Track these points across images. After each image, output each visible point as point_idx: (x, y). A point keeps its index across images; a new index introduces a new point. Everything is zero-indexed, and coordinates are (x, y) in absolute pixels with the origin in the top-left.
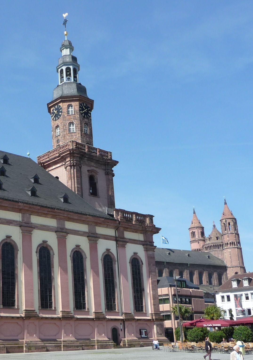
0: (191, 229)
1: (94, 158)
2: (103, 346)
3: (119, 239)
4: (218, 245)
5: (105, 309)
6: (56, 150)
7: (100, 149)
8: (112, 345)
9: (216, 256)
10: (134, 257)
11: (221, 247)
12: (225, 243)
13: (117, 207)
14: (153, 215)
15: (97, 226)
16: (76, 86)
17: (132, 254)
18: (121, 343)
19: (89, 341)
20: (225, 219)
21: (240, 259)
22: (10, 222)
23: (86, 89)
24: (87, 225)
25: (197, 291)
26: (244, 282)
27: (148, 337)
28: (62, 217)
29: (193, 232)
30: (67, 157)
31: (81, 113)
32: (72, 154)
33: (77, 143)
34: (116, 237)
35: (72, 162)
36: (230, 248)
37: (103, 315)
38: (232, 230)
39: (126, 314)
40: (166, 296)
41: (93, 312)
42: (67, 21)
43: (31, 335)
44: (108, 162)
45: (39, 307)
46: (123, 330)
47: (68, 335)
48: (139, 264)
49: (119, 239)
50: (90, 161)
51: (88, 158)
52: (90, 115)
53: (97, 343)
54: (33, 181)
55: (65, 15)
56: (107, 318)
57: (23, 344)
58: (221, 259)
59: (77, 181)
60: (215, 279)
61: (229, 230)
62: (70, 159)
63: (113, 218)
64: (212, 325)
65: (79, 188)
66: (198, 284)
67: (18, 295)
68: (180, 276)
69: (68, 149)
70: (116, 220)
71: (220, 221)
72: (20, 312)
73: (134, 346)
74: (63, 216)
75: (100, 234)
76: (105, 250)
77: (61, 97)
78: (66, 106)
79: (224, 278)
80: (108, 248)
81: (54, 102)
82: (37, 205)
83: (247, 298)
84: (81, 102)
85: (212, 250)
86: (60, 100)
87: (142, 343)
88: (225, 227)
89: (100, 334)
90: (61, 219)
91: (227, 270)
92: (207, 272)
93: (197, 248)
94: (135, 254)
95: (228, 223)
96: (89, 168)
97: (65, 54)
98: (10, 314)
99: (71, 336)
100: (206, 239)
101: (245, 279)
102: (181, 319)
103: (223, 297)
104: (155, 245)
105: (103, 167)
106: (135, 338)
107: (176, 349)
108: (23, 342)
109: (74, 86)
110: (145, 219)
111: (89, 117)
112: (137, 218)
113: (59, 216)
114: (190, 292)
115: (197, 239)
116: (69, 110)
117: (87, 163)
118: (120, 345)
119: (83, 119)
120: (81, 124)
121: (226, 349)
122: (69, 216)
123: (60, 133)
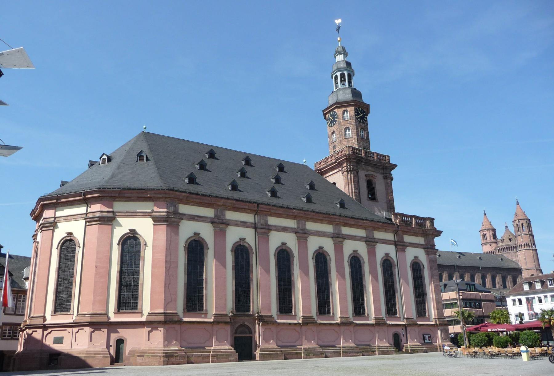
0: (482, 231)
1: (371, 162)
2: (384, 352)
4: (511, 247)
5: (386, 314)
6: (333, 156)
10: (414, 261)
14: (433, 218)
15: (374, 231)
17: (413, 258)
18: (403, 348)
19: (370, 347)
20: (518, 220)
24: (332, 226)
25: (473, 293)
26: (536, 285)
28: (338, 223)
29: (484, 234)
30: (344, 163)
32: (348, 159)
33: (353, 148)
34: (395, 241)
35: (348, 167)
36: (524, 250)
37: (384, 320)
38: (526, 231)
39: (408, 319)
40: (454, 301)
41: (373, 317)
43: (309, 341)
44: (386, 166)
45: (317, 313)
46: (405, 336)
47: (347, 341)
48: (420, 268)
51: (365, 162)
52: (366, 119)
53: (378, 349)
56: (388, 323)
57: (301, 350)
58: (515, 261)
61: (522, 231)
62: (347, 164)
63: (392, 222)
65: (356, 193)
67: (295, 301)
68: (461, 280)
69: (344, 155)
70: (395, 224)
71: (513, 222)
72: (297, 318)
73: (417, 352)
75: (378, 239)
76: (384, 255)
77: (335, 104)
78: (342, 112)
83: (540, 301)
85: (505, 252)
86: (335, 106)
87: (426, 349)
88: (518, 229)
89: (381, 339)
90: (337, 224)
92: (500, 275)
95: (521, 224)
96: (367, 173)
97: (339, 60)
98: (287, 321)
99: (350, 342)
101: (537, 282)
102: (464, 323)
103: (514, 300)
104: (436, 248)
105: (382, 171)
106: (418, 344)
108: (301, 348)
109: (349, 91)
112: (417, 221)
115: (489, 242)
116: (344, 115)
118: (402, 351)
119: (359, 124)
120: (357, 128)
121: (510, 355)
122: (345, 221)
123: (336, 139)
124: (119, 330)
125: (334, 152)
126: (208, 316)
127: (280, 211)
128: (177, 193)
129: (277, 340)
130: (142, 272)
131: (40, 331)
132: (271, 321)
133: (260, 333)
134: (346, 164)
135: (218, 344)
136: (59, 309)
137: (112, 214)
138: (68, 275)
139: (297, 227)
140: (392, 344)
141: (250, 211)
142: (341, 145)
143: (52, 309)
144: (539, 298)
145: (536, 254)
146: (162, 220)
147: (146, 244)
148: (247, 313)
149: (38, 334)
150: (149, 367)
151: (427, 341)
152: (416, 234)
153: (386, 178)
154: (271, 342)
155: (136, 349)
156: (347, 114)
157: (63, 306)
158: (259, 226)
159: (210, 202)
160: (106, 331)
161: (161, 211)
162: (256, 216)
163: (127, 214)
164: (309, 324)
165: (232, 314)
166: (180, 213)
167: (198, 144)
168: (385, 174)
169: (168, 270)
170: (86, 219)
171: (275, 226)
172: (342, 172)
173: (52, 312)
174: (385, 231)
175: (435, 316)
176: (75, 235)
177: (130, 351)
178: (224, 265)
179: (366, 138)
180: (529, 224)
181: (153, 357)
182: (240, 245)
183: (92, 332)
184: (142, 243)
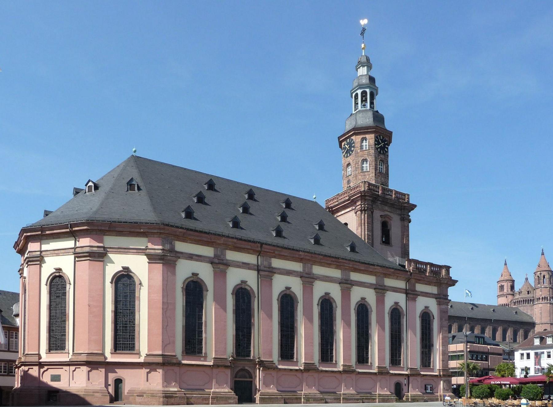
2: (384, 399)
3: (410, 292)
4: (528, 300)
5: (390, 364)
9: (524, 312)
12: (536, 298)
13: (411, 257)
14: (450, 266)
15: (385, 278)
16: (372, 115)
18: (404, 397)
19: (370, 395)
23: (383, 117)
24: (375, 277)
27: (433, 392)
29: (501, 285)
30: (358, 201)
31: (376, 148)
32: (363, 196)
33: (370, 184)
34: (406, 290)
35: (363, 205)
36: (541, 303)
37: (387, 370)
41: (376, 366)
43: (310, 387)
44: (405, 206)
47: (348, 388)
49: (410, 292)
50: (384, 205)
51: (382, 201)
52: (387, 150)
54: (317, 228)
56: (391, 372)
57: (301, 396)
60: (520, 336)
61: (543, 283)
62: (361, 203)
63: (404, 269)
64: (501, 382)
65: (369, 235)
66: (501, 341)
67: (297, 348)
69: (359, 191)
70: (408, 271)
71: (534, 273)
72: (299, 364)
73: (418, 401)
75: (388, 287)
77: (354, 129)
78: (360, 140)
80: (397, 301)
81: (346, 135)
82: (308, 252)
84: (377, 134)
85: (520, 305)
86: (353, 132)
87: (426, 399)
89: (382, 388)
90: (346, 269)
92: (512, 328)
93: (505, 303)
94: (427, 307)
96: (382, 213)
97: (362, 74)
100: (515, 293)
101: (549, 337)
104: (449, 298)
105: (399, 212)
106: (420, 393)
107: (458, 405)
108: (302, 394)
109: (370, 114)
110: (441, 270)
111: (386, 153)
112: (432, 269)
113: (343, 266)
114: (488, 348)
115: (506, 293)
116: (363, 144)
117: (380, 207)
120: (376, 161)
122: (355, 266)
123: (351, 173)
125: (348, 187)
126: (208, 359)
127: (285, 253)
128: (173, 228)
129: (278, 385)
130: (138, 313)
131: (36, 368)
133: (261, 378)
135: (218, 386)
137: (102, 249)
138: (61, 313)
139: (303, 271)
144: (548, 353)
147: (141, 284)
148: (247, 358)
149: (34, 371)
151: (429, 391)
152: (429, 283)
158: (262, 268)
159: (210, 240)
161: (157, 248)
162: (259, 256)
163: (119, 250)
168: (402, 216)
169: (166, 311)
171: (279, 269)
172: (355, 211)
173: (46, 350)
174: (397, 278)
175: (439, 367)
178: (224, 308)
179: (384, 173)
183: (89, 372)
184: (137, 283)
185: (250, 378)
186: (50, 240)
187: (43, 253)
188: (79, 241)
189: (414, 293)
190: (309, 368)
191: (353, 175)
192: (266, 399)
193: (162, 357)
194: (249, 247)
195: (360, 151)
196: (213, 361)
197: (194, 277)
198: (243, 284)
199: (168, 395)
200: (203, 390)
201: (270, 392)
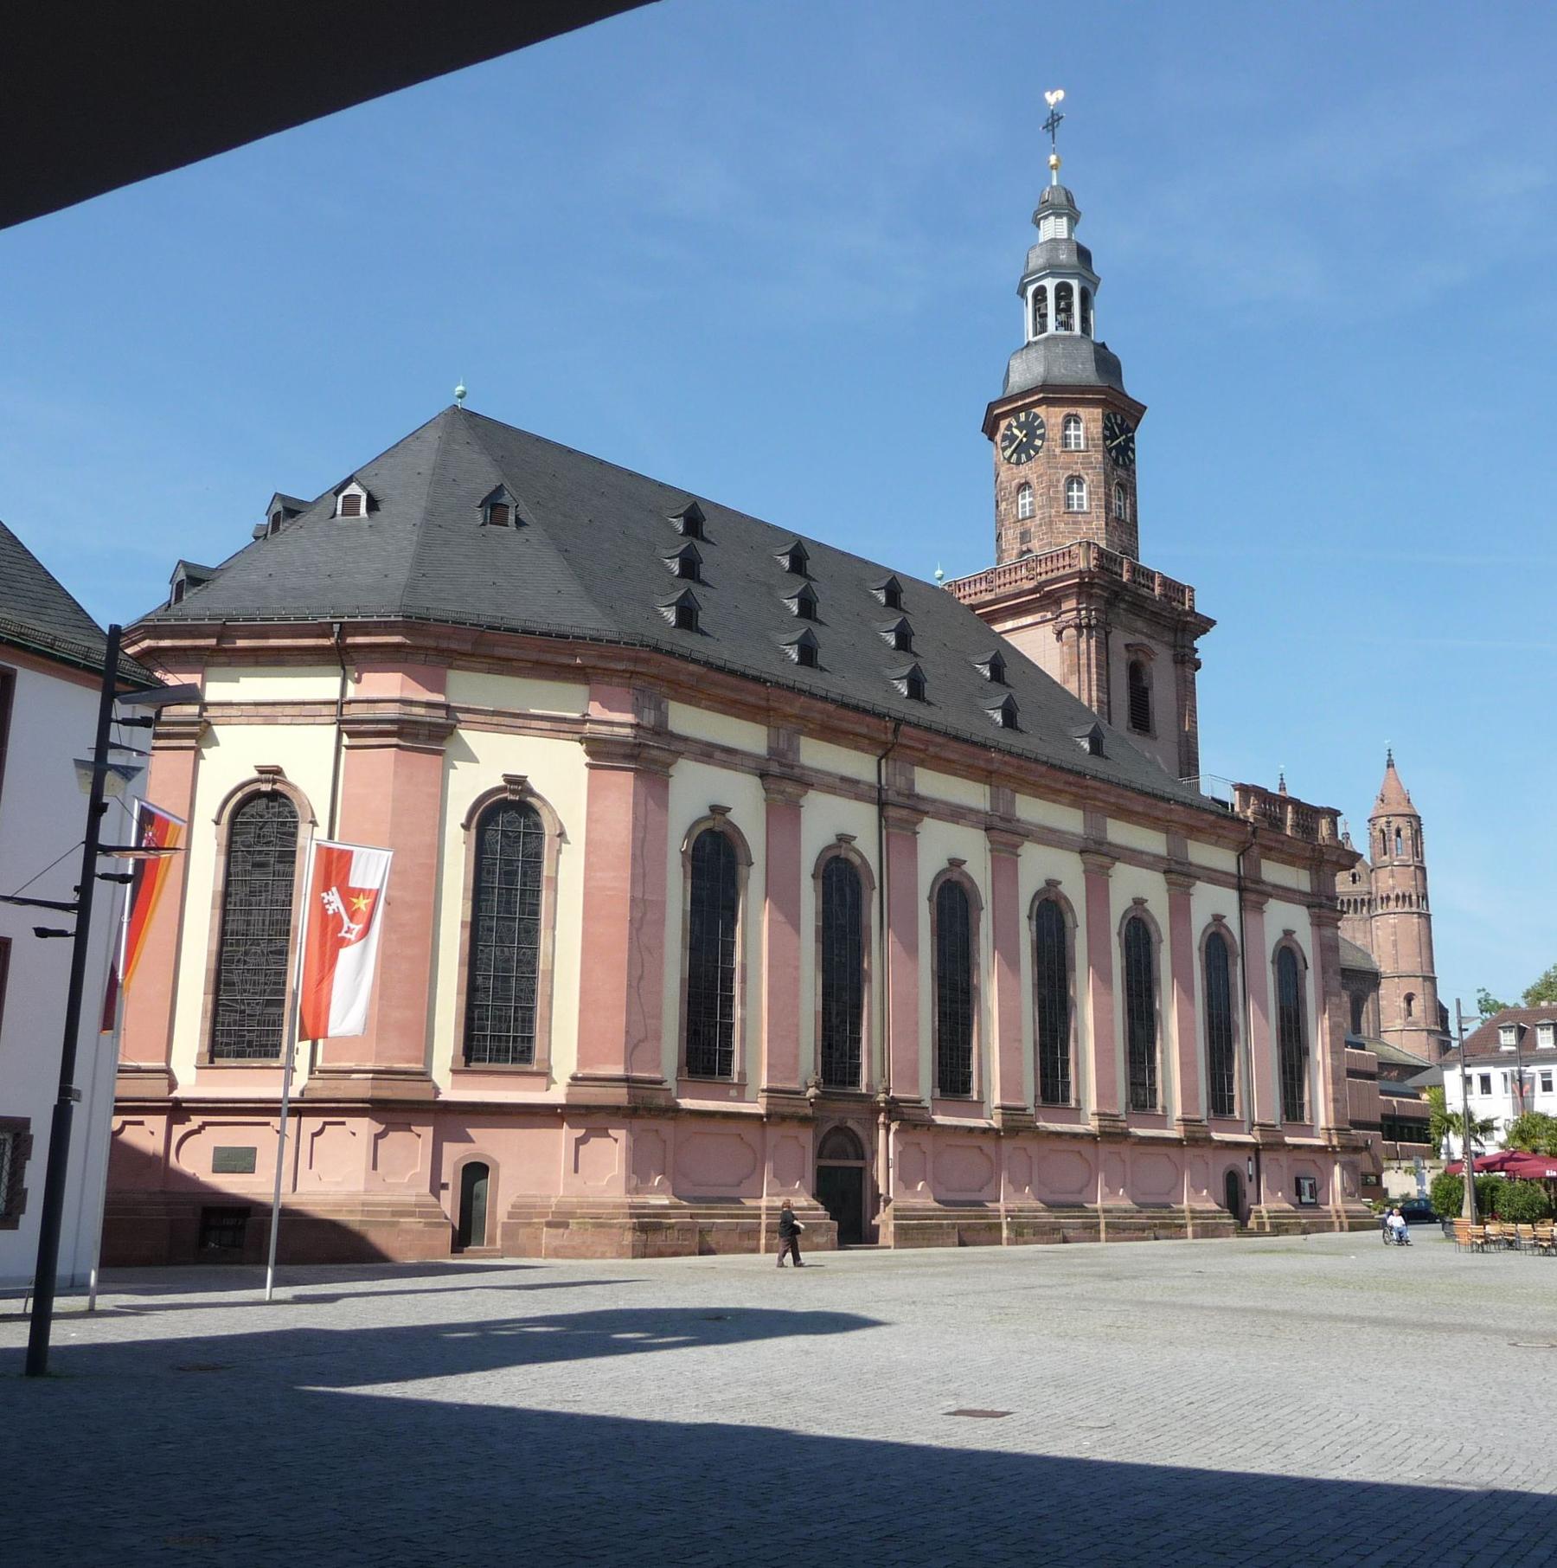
1: (1146, 605)
2: (1208, 1230)
4: (1356, 901)
7: (1163, 577)
8: (1230, 1225)
11: (1365, 909)
19: (1170, 1212)
21: (1425, 951)
22: (961, 813)
28: (1101, 804)
30: (1067, 596)
32: (1084, 587)
33: (1101, 553)
35: (1083, 612)
36: (1395, 913)
42: (1058, 120)
45: (1036, 1097)
46: (1254, 1178)
49: (1250, 885)
50: (1134, 614)
53: (1193, 1218)
55: (1054, 97)
57: (999, 1217)
58: (1362, 948)
59: (1098, 680)
62: (1078, 603)
65: (1102, 702)
67: (980, 1056)
71: (1369, 821)
73: (1287, 1232)
74: (1104, 801)
76: (1210, 919)
77: (1043, 387)
78: (1060, 420)
79: (1367, 1013)
81: (1016, 401)
86: (1041, 396)
88: (1385, 845)
91: (1379, 984)
95: (1394, 832)
96: (1130, 639)
99: (919, 1188)
101: (1542, 1026)
103: (1468, 1080)
105: (1169, 637)
106: (1287, 1206)
109: (1086, 351)
116: (1067, 432)
120: (1107, 484)
122: (1121, 801)
123: (1032, 511)
124: (471, 1132)
126: (748, 1094)
127: (953, 752)
128: (674, 662)
129: (936, 1183)
130: (549, 931)
131: (158, 1123)
132: (918, 1118)
133: (891, 1156)
134: (1075, 601)
135: (778, 1189)
136: (228, 1044)
137: (442, 713)
138: (267, 923)
139: (992, 810)
140: (1222, 1203)
141: (869, 744)
142: (1052, 532)
143: (200, 1045)
144: (1543, 1075)
145: (1427, 931)
146: (622, 751)
147: (561, 835)
148: (850, 1090)
149: (148, 1135)
150: (582, 1262)
151: (1306, 1198)
152: (1291, 860)
153: (1183, 662)
154: (656, 1184)
155: (534, 1200)
156: (1077, 429)
157: (244, 1036)
158: (891, 796)
159: (763, 703)
160: (428, 1132)
161: (618, 720)
162: (883, 761)
163: (495, 720)
164: (1022, 1131)
165: (818, 1092)
166: (675, 731)
167: (630, 475)
168: (1178, 649)
169: (638, 930)
170: (341, 722)
171: (933, 801)
172: (1060, 627)
173: (200, 1055)
174: (1216, 842)
175: (1327, 1121)
176: (291, 775)
177: (513, 1206)
178: (794, 922)
179: (1128, 520)
180: (1416, 831)
181: (599, 1230)
182: (837, 858)
183: (378, 1137)
184: (549, 830)
185: (858, 1159)
186: (238, 669)
187: (212, 712)
188: (358, 681)
189: (1257, 887)
190: (1014, 1124)
191: (1041, 519)
192: (913, 1229)
193: (628, 1087)
194: (864, 730)
195: (1062, 452)
196: (764, 1101)
197: (718, 817)
198: (844, 845)
199: (646, 1220)
200: (737, 1200)
201: (919, 1206)
